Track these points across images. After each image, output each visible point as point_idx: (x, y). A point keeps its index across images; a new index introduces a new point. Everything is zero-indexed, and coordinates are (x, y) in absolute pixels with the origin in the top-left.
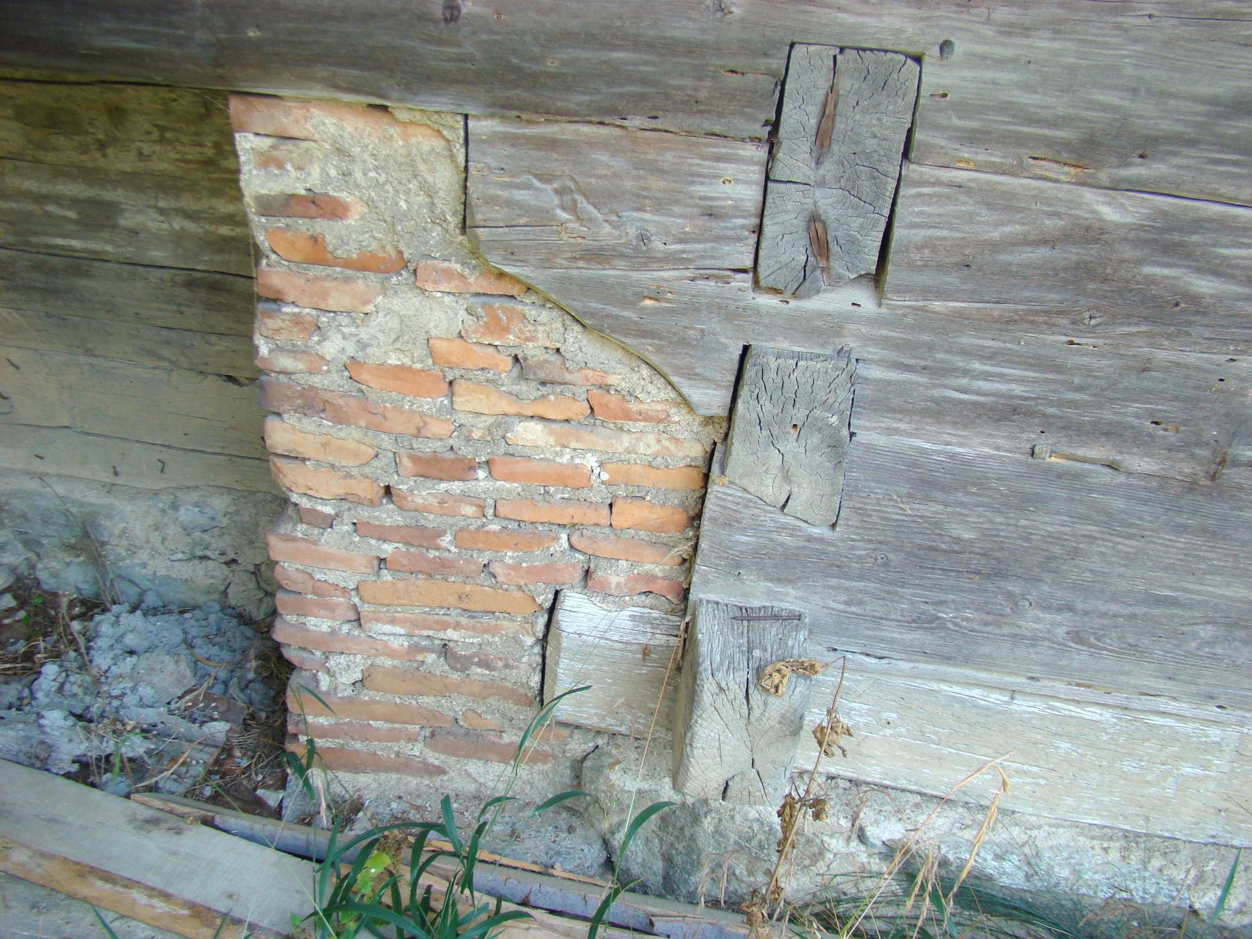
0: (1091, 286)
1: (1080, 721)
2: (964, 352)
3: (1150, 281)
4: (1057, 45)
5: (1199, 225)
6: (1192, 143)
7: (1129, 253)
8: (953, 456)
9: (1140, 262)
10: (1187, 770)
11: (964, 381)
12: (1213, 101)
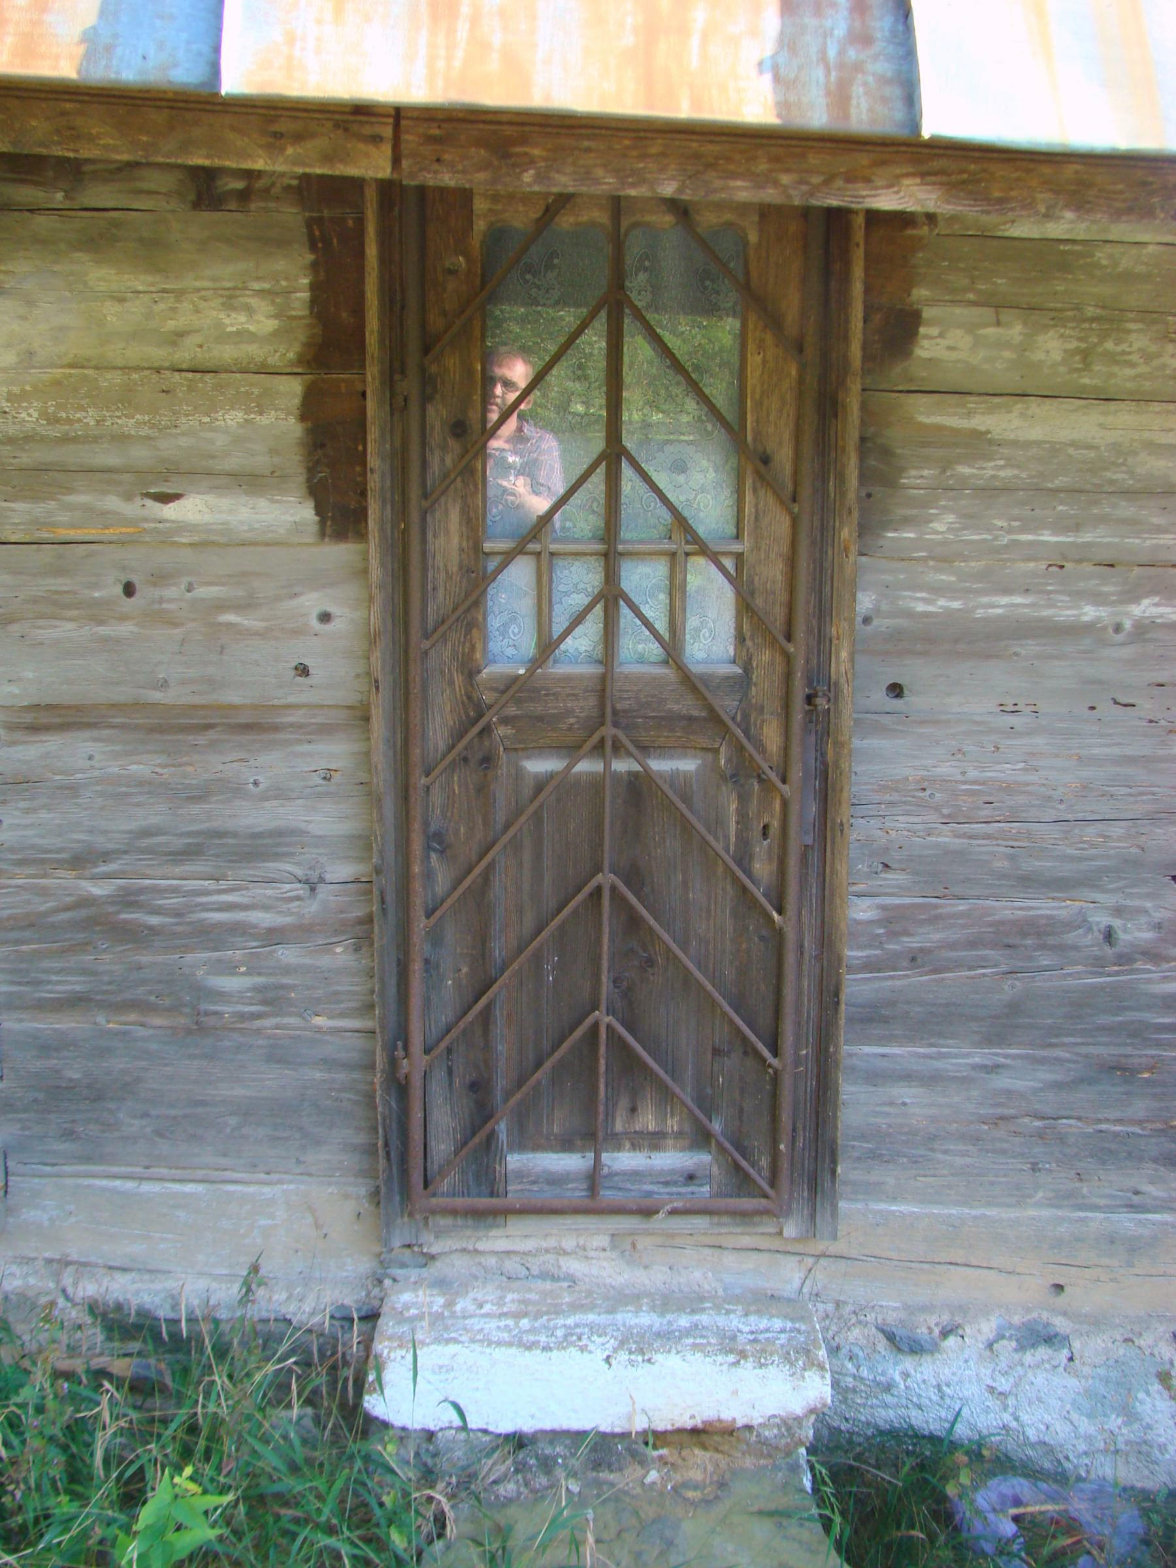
0: (97, 928)
1: (185, 1195)
2: (44, 971)
3: (126, 922)
4: (51, 815)
5: (142, 890)
6: (126, 852)
7: (111, 909)
8: (56, 1030)
9: (119, 912)
10: (263, 1222)
11: (49, 987)
12: (130, 832)
